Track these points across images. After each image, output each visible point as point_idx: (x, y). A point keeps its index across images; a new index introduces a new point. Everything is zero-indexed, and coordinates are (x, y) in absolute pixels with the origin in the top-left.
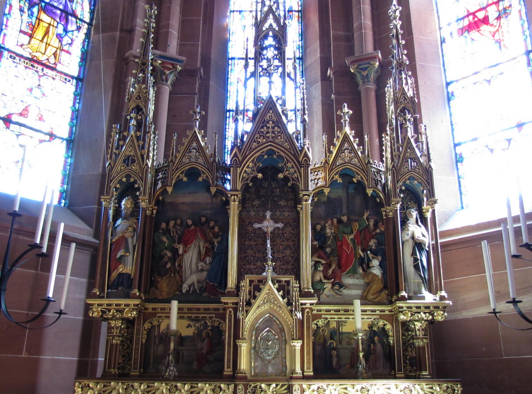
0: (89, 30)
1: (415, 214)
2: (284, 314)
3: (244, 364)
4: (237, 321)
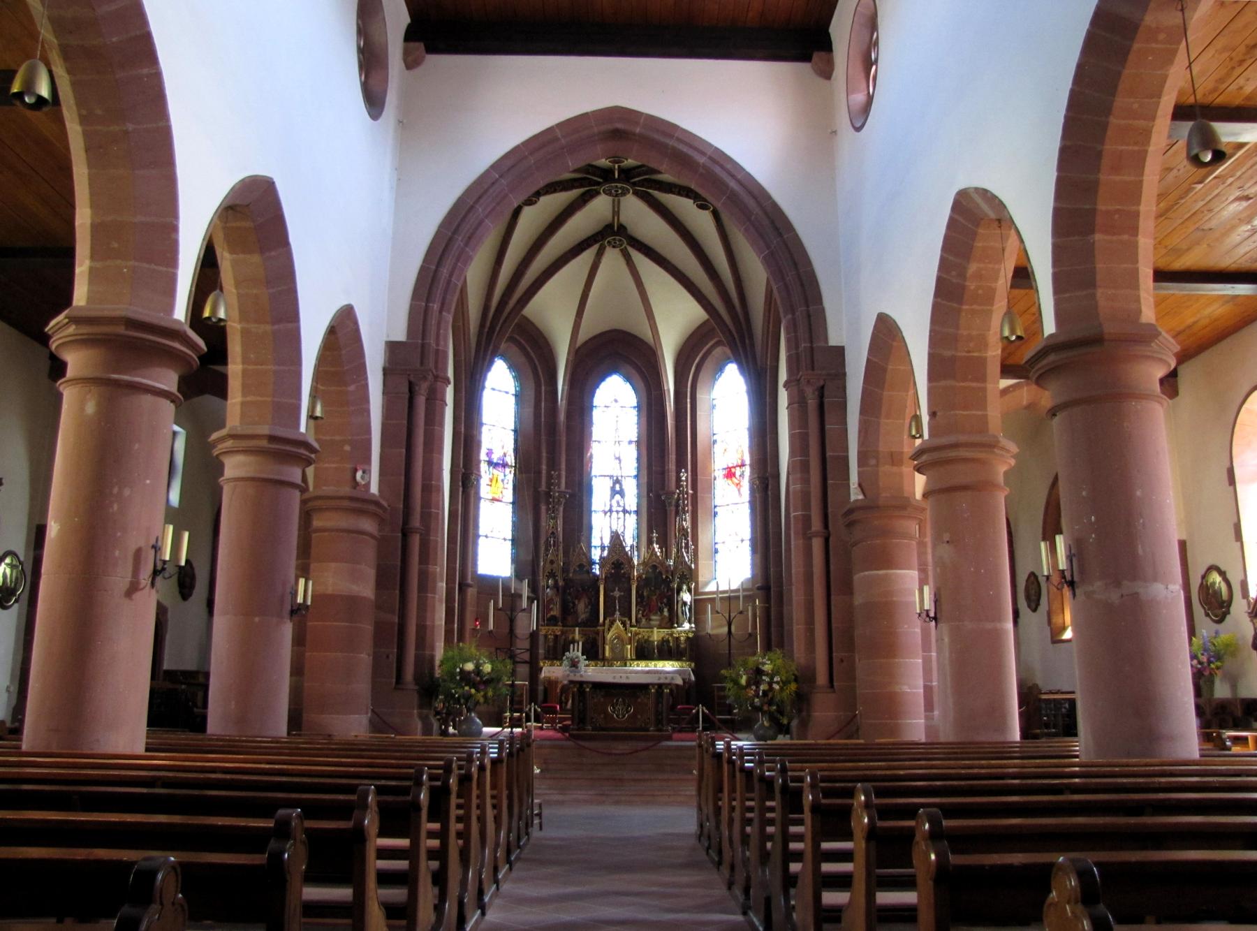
2: (623, 634)
3: (607, 654)
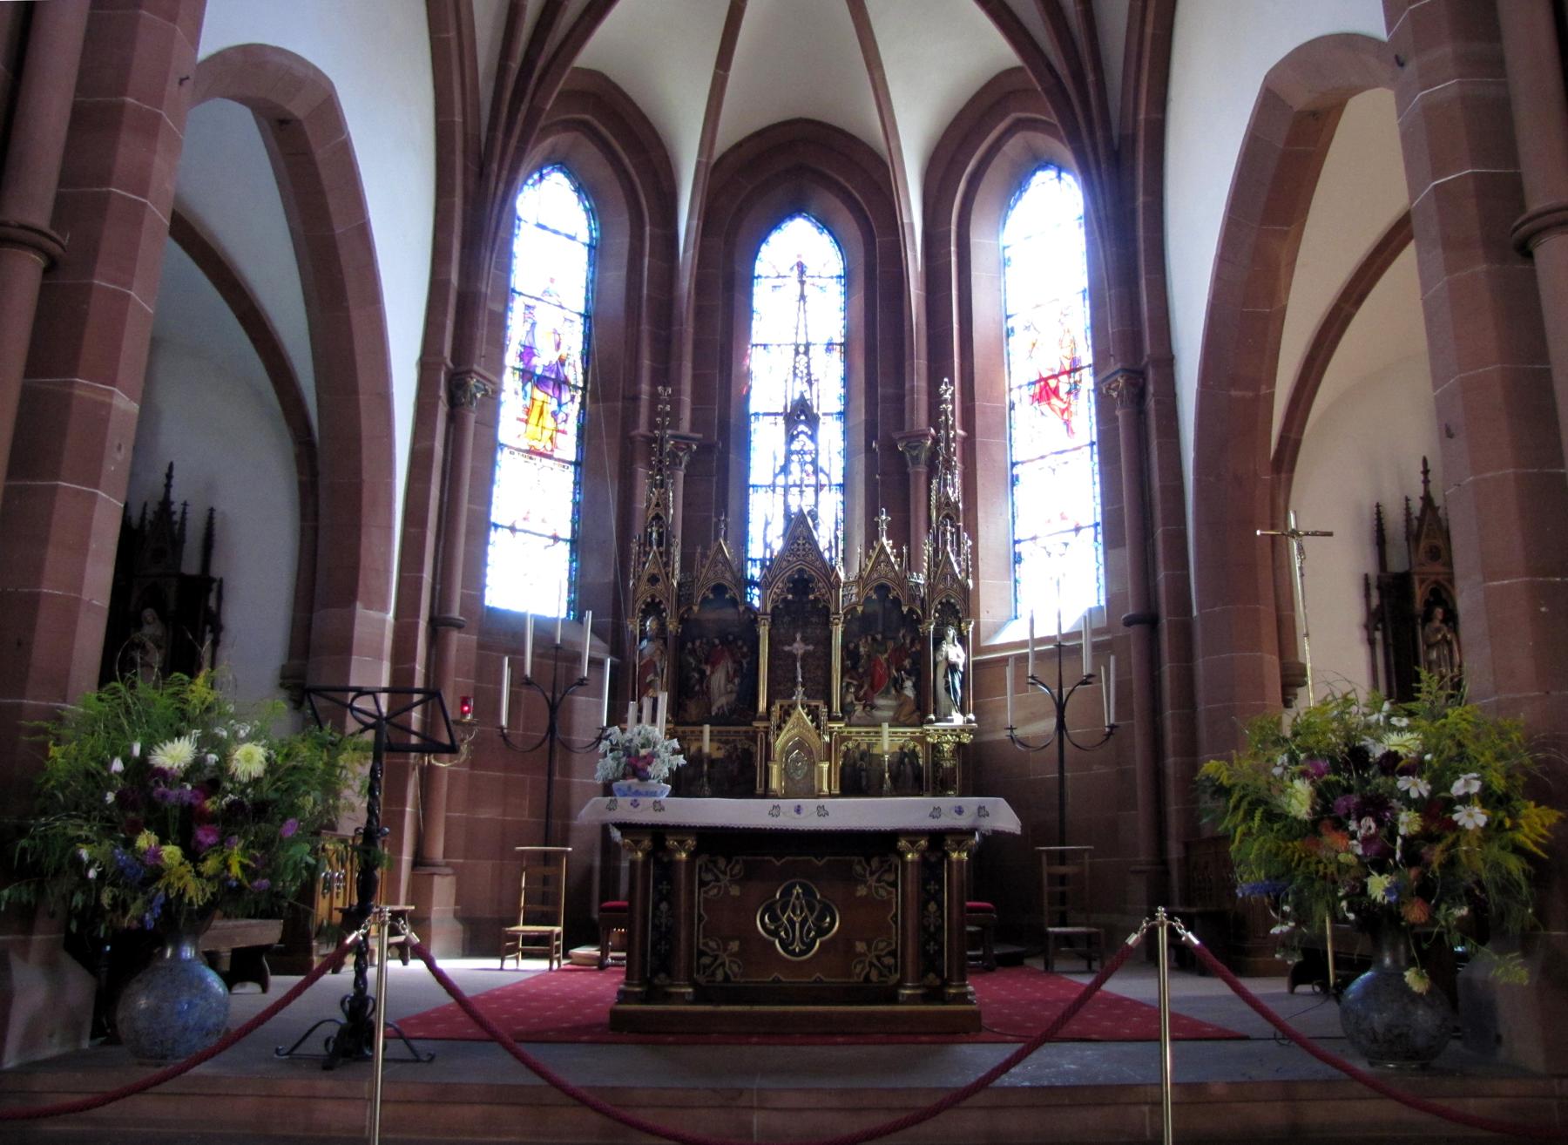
0: (583, 397)
1: (952, 632)
2: (812, 737)
4: (768, 745)
